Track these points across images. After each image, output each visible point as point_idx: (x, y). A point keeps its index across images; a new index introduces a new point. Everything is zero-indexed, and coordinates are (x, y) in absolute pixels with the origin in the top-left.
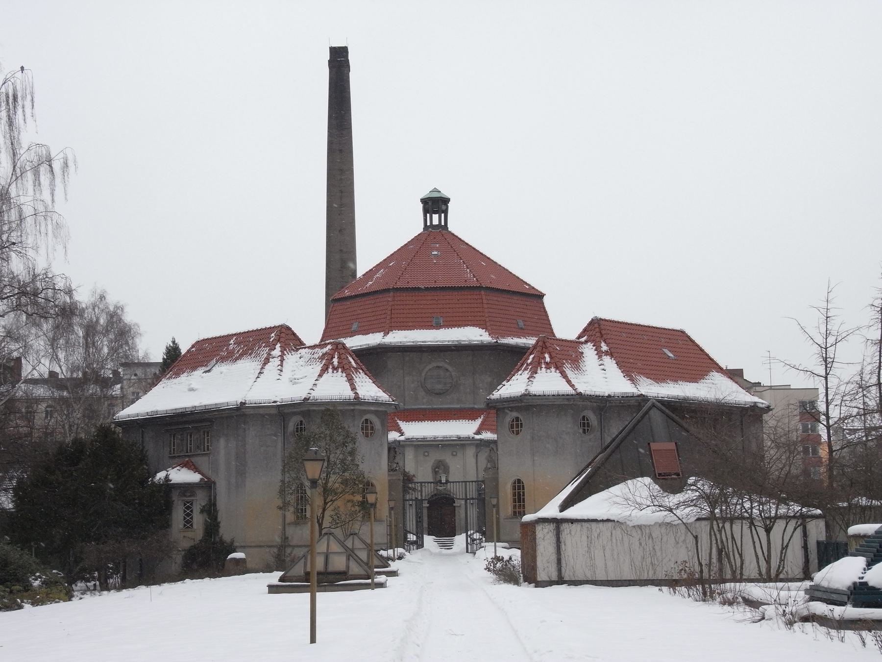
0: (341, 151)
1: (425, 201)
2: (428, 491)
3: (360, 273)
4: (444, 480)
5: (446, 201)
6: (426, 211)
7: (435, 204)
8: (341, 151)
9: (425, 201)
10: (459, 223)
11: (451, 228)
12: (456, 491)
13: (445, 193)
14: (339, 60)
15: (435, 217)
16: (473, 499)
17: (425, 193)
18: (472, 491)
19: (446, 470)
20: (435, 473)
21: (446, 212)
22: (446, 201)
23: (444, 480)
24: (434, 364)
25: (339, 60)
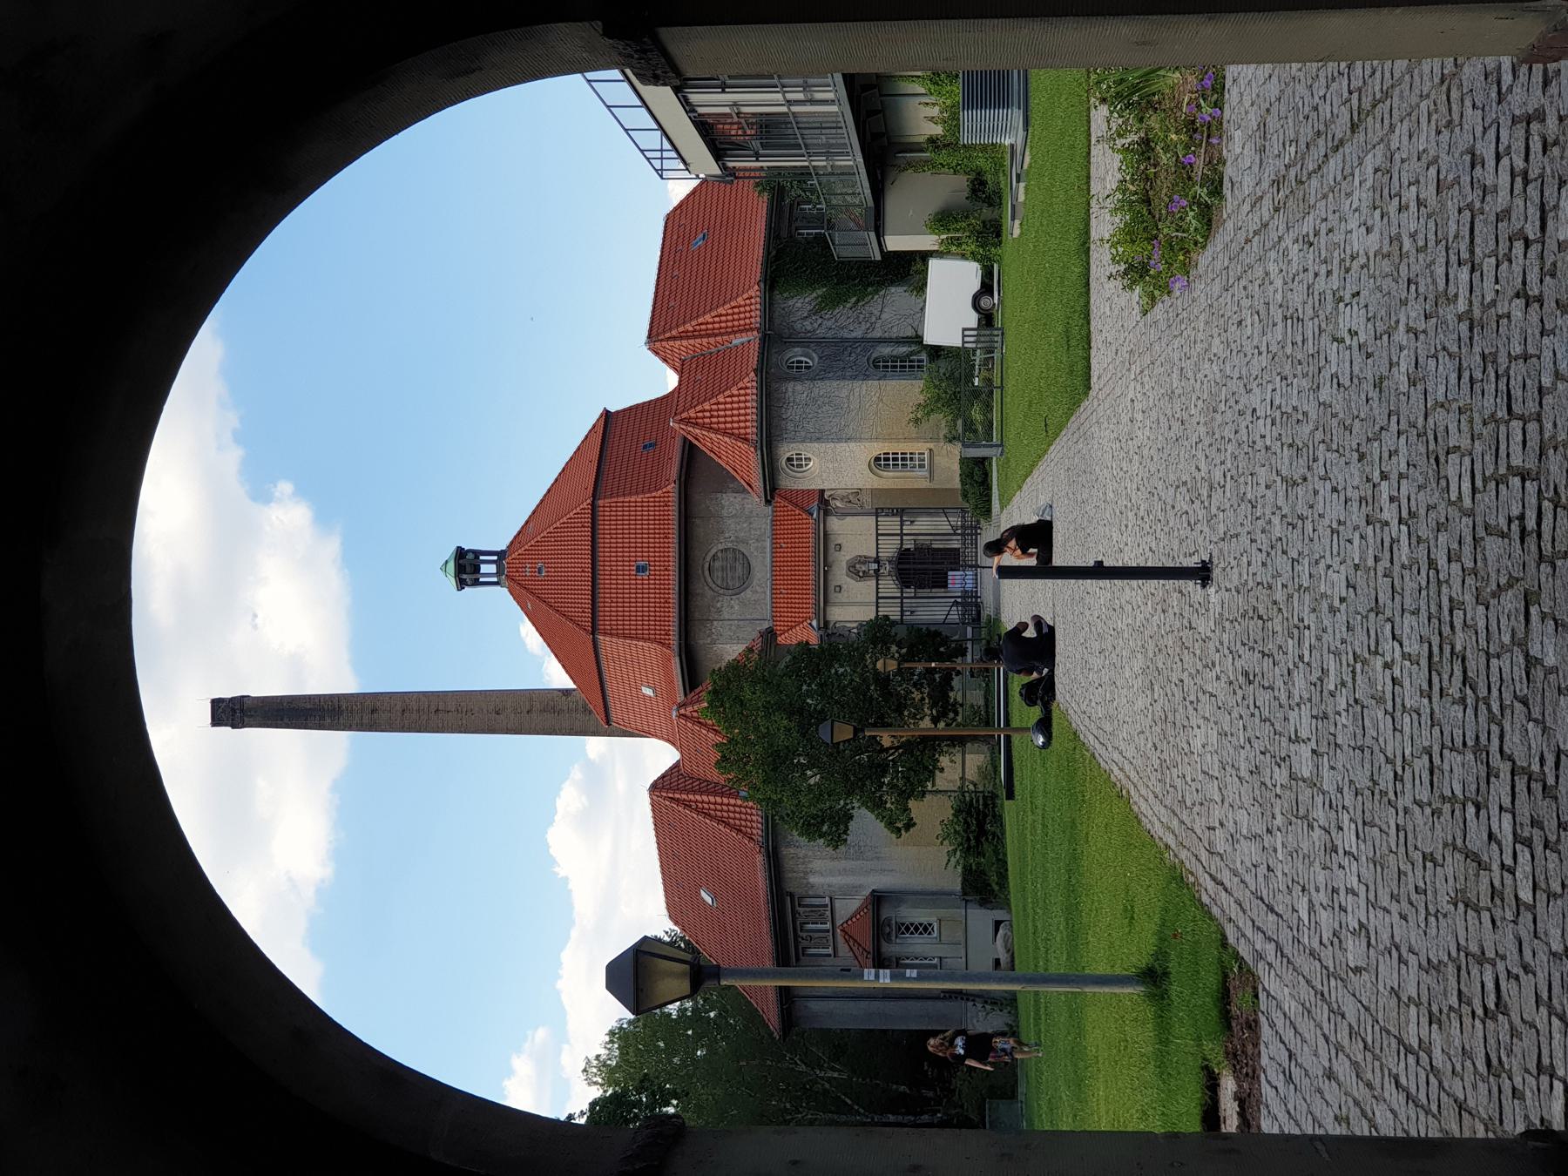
1: (461, 584)
2: (890, 586)
3: (571, 685)
4: (875, 566)
5: (461, 553)
6: (476, 583)
7: (466, 567)
8: (373, 711)
9: (461, 584)
11: (502, 546)
12: (890, 548)
13: (449, 552)
15: (484, 568)
16: (902, 522)
17: (451, 582)
18: (890, 524)
19: (864, 560)
20: (866, 575)
21: (477, 553)
22: (461, 553)
23: (875, 566)
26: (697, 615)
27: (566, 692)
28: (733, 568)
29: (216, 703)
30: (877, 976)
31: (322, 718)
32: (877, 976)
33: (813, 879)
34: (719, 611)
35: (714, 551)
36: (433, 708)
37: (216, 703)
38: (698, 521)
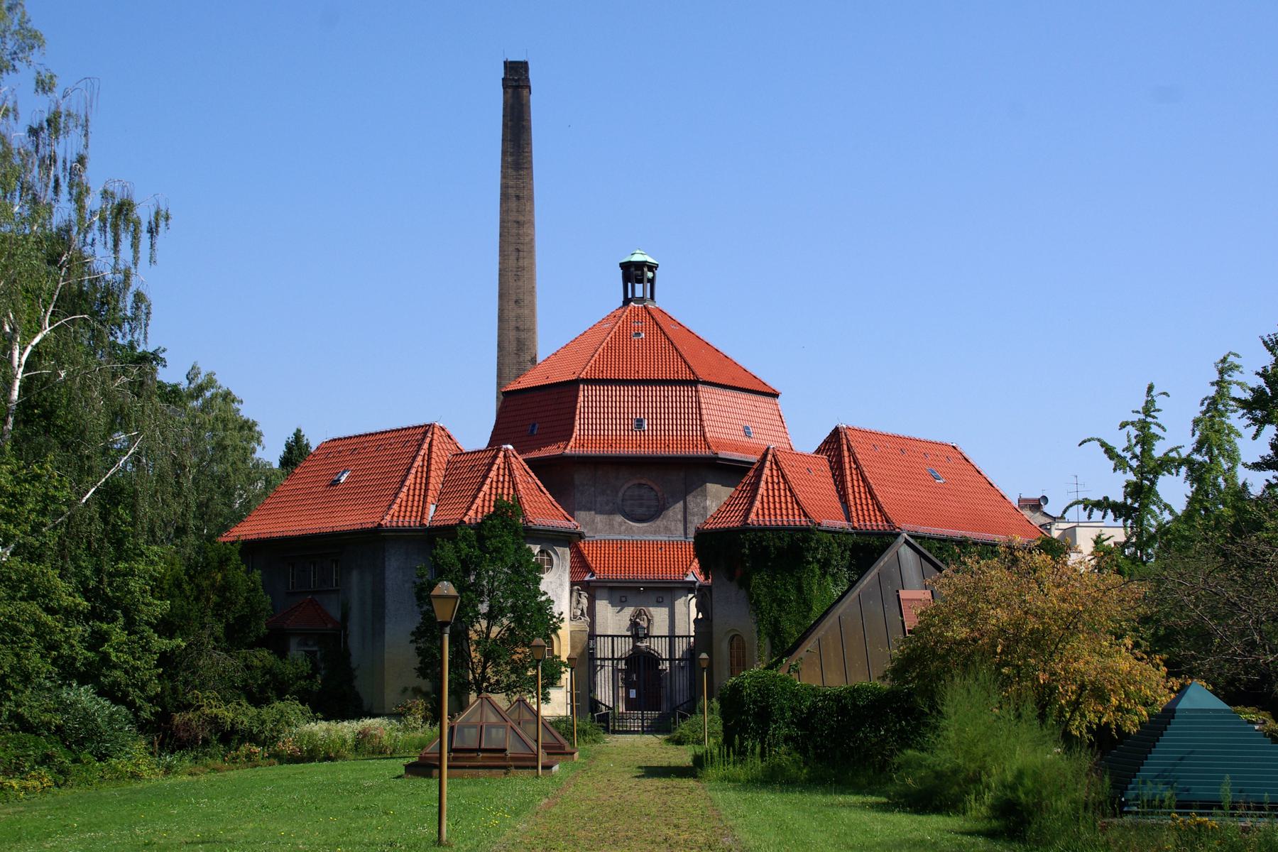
0: (518, 197)
8: (518, 197)
10: (671, 297)
14: (516, 78)
24: (636, 482)
25: (516, 78)
27: (533, 360)
28: (641, 505)
31: (512, 154)
33: (355, 576)
35: (656, 488)
36: (521, 247)
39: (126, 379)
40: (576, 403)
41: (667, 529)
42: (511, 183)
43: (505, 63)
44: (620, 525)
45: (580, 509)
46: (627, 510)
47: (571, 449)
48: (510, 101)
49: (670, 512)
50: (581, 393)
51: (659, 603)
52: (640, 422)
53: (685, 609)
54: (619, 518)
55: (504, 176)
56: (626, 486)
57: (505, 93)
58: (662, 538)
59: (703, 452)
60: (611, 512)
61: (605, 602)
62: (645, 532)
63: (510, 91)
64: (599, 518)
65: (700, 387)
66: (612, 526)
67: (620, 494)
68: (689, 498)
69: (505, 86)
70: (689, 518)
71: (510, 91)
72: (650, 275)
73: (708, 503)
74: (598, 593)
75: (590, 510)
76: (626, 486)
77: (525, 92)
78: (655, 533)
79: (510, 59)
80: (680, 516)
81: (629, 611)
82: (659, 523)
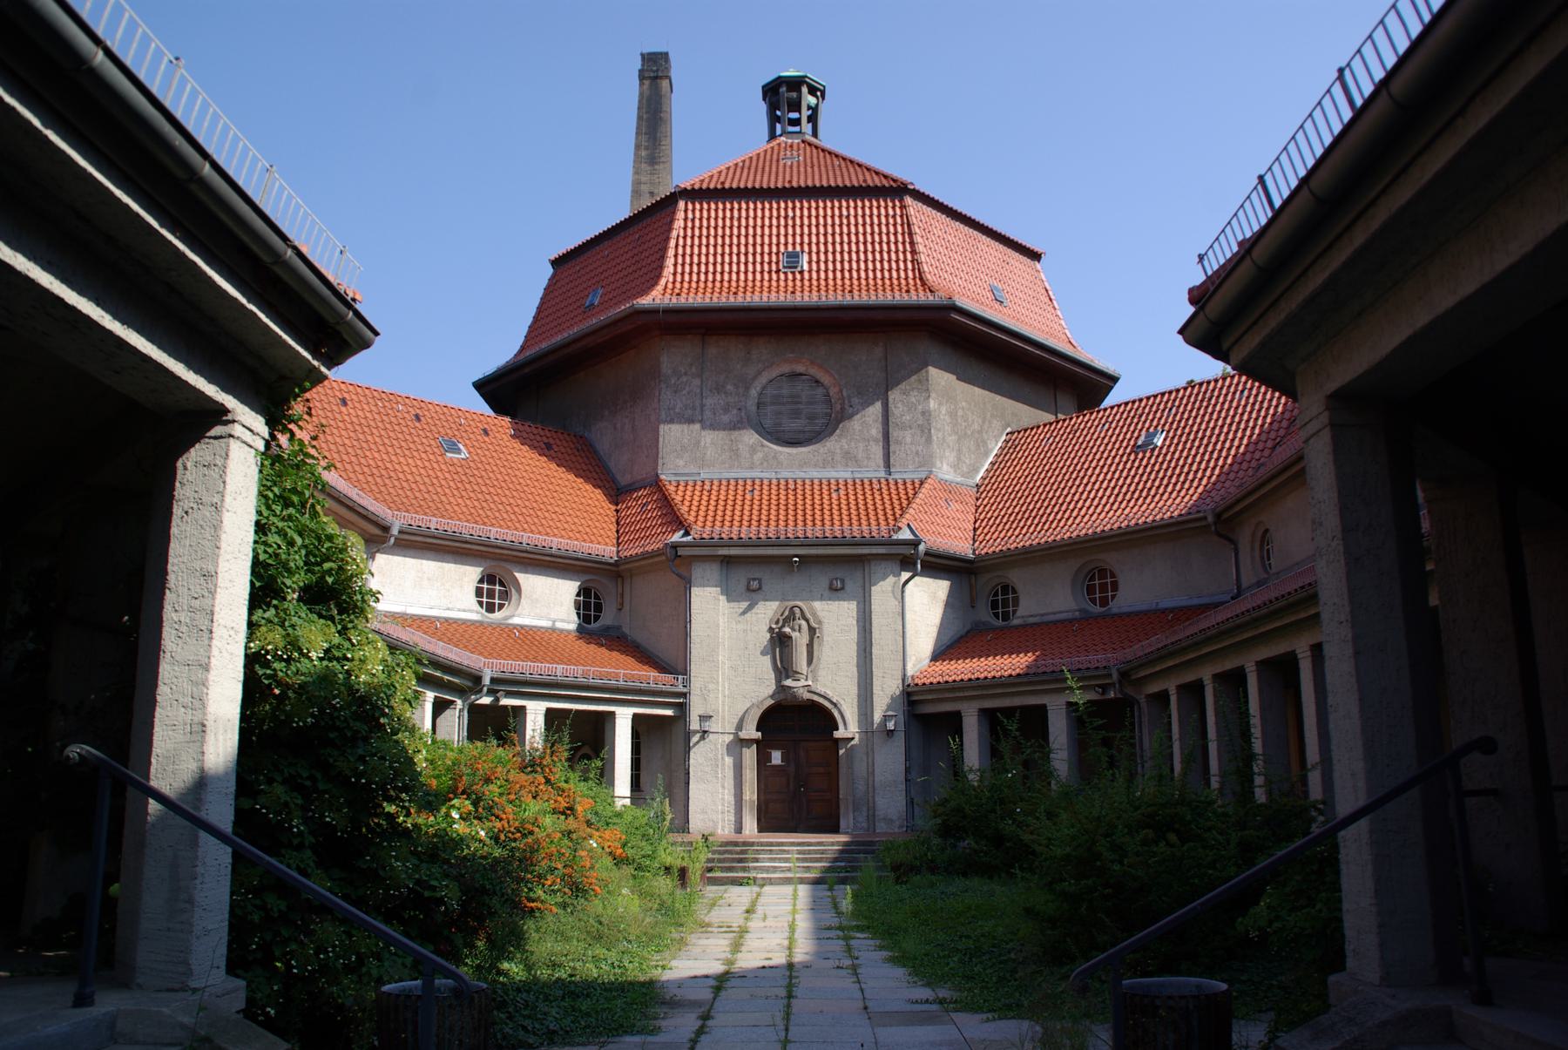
14: (655, 69)
24: (786, 369)
25: (655, 69)
26: (712, 351)
28: (796, 414)
29: (664, 56)
30: (1487, 746)
31: (647, 148)
32: (1487, 746)
34: (719, 389)
35: (825, 379)
37: (664, 56)
38: (878, 351)
39: (973, 845)
40: (670, 229)
41: (849, 458)
42: (643, 179)
43: (643, 55)
44: (753, 450)
45: (671, 421)
46: (768, 423)
47: (655, 298)
48: (647, 93)
49: (855, 424)
50: (680, 215)
51: (835, 591)
52: (794, 257)
53: (894, 604)
54: (750, 437)
55: (636, 173)
56: (763, 379)
57: (641, 84)
58: (843, 474)
59: (919, 297)
60: (734, 426)
61: (713, 591)
62: (803, 464)
63: (647, 82)
64: (710, 438)
65: (908, 200)
66: (735, 454)
67: (754, 392)
68: (894, 395)
69: (642, 77)
70: (895, 434)
71: (647, 82)
72: (812, 100)
73: (932, 404)
74: (698, 571)
75: (691, 421)
76: (763, 379)
77: (665, 83)
78: (825, 464)
79: (645, 51)
80: (875, 431)
81: (767, 611)
82: (832, 445)
